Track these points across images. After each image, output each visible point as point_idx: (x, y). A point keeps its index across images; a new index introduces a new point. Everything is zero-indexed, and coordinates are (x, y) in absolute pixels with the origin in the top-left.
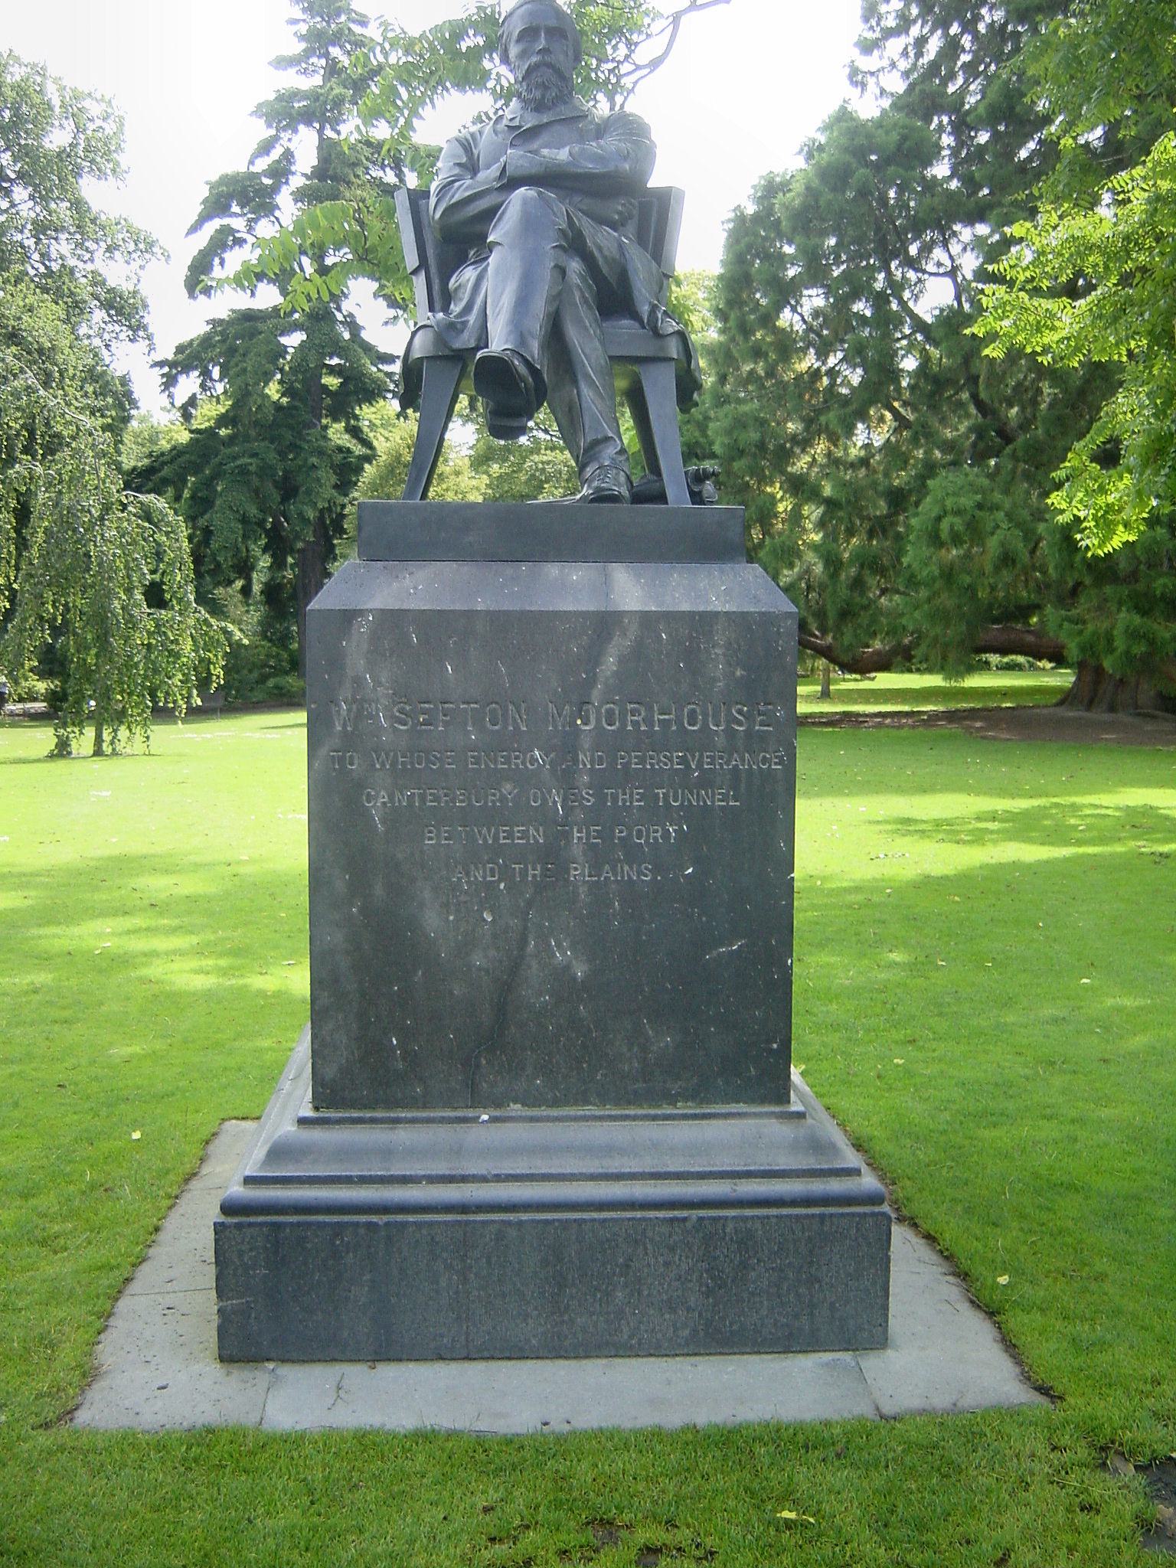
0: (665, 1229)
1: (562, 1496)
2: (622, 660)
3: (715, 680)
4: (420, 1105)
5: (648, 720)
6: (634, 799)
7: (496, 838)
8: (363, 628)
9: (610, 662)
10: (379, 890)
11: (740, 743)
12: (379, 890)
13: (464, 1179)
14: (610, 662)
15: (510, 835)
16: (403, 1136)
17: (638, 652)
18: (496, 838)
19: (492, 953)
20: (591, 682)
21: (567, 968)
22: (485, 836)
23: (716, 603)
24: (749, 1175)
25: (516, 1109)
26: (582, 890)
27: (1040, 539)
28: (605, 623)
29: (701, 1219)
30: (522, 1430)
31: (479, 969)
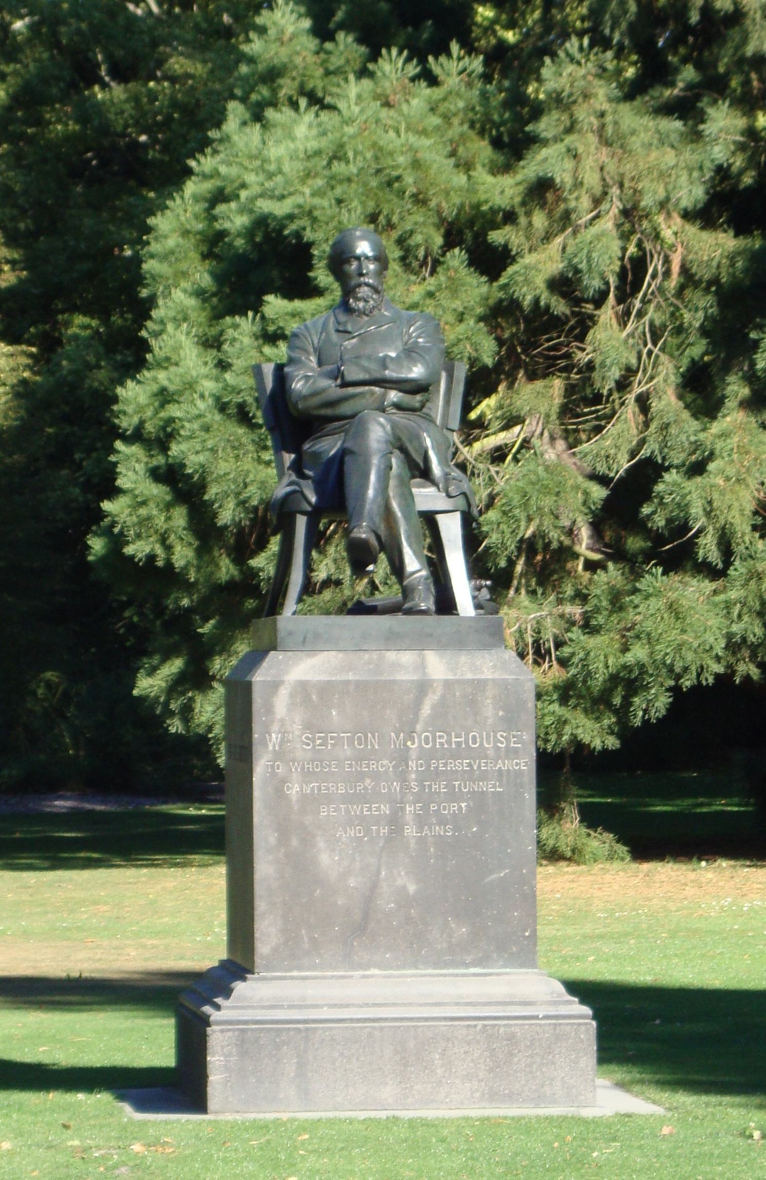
2: (434, 707)
3: (487, 718)
5: (449, 742)
7: (362, 812)
11: (503, 754)
14: (426, 710)
20: (416, 720)
21: (404, 887)
22: (356, 810)
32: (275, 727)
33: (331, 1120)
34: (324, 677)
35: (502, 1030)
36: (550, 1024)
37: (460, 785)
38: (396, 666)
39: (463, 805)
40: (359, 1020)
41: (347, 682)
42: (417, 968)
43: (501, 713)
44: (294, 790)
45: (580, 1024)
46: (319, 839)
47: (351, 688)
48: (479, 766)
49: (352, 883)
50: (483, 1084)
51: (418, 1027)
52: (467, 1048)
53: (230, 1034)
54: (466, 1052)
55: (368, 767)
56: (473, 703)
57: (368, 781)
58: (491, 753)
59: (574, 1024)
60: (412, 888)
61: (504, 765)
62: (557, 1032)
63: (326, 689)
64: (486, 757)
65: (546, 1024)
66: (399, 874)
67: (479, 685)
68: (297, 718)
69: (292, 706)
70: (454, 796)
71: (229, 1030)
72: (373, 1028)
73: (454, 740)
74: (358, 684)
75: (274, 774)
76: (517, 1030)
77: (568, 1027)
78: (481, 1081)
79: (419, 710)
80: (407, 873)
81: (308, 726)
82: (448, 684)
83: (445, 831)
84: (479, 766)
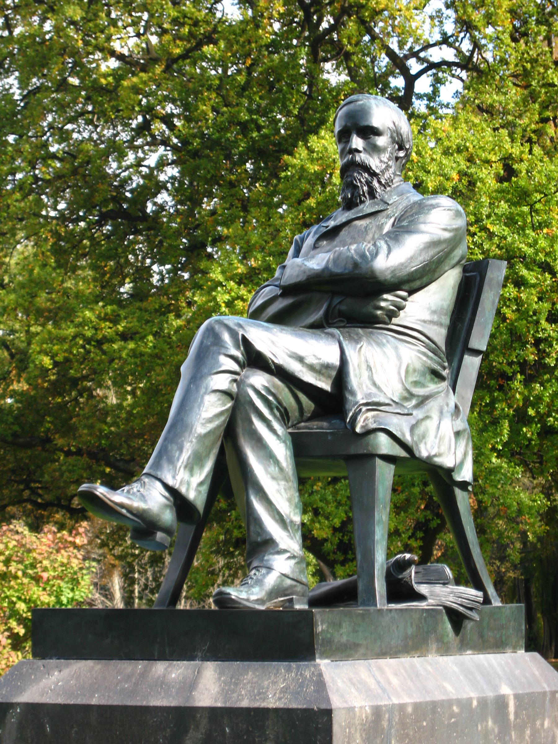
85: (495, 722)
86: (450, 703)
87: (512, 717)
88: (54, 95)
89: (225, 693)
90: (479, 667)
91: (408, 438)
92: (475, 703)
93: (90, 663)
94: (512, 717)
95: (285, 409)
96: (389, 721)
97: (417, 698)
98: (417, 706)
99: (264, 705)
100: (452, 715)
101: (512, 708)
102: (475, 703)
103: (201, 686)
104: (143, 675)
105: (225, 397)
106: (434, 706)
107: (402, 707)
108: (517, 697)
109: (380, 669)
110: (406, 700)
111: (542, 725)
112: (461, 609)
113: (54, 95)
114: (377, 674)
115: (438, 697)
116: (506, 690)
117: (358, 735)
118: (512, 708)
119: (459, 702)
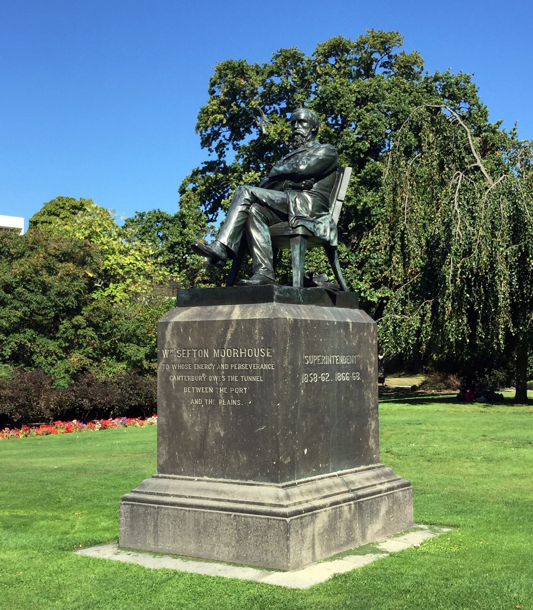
0: (226, 518)
1: (89, 581)
2: (232, 335)
3: (256, 340)
4: (331, 470)
5: (239, 354)
6: (234, 378)
7: (201, 391)
8: (170, 327)
9: (229, 336)
10: (173, 406)
11: (263, 361)
12: (173, 406)
13: (181, 496)
14: (229, 336)
15: (204, 390)
16: (172, 483)
17: (235, 333)
18: (201, 391)
19: (200, 427)
20: (224, 342)
21: (219, 433)
22: (198, 390)
23: (258, 316)
24: (254, 503)
25: (206, 478)
26: (223, 408)
27: (54, 351)
28: (227, 323)
29: (235, 515)
30: (301, 587)
31: (197, 432)
32: (166, 346)
33: (124, 564)
34: (186, 320)
35: (243, 518)
36: (266, 518)
37: (244, 378)
38: (220, 313)
39: (245, 389)
40: (338, 494)
41: (196, 322)
42: (224, 478)
43: (262, 338)
44: (174, 379)
45: (280, 520)
46: (183, 404)
47: (197, 325)
48: (252, 367)
49: (197, 429)
50: (234, 549)
51: (205, 512)
52: (227, 528)
53: (127, 506)
54: (227, 529)
55: (204, 367)
56: (250, 334)
57: (204, 375)
58: (257, 360)
59: (277, 520)
60: (222, 433)
61: (266, 367)
62: (269, 523)
63: (187, 325)
64: (255, 362)
65: (264, 518)
66: (217, 426)
67: (252, 322)
68: (175, 341)
69: (173, 335)
70: (241, 384)
71: (127, 504)
72: (186, 510)
73: (241, 353)
74: (200, 323)
75: (165, 370)
76: (250, 520)
77: (275, 521)
78: (233, 547)
79: (226, 336)
80: (220, 426)
81: (179, 346)
82: (238, 322)
83: (237, 403)
84: (252, 367)
85: (344, 330)
86: (326, 321)
87: (351, 330)
88: (460, 270)
89: (242, 315)
90: (339, 313)
91: (312, 230)
92: (336, 323)
93: (197, 307)
94: (351, 330)
95: (267, 218)
96: (301, 324)
97: (312, 318)
98: (311, 321)
99: (255, 318)
100: (327, 326)
101: (351, 327)
102: (336, 323)
103: (234, 313)
104: (215, 310)
105: (245, 214)
106: (319, 322)
107: (306, 321)
108: (353, 323)
109: (299, 308)
110: (308, 318)
111: (364, 334)
112: (331, 291)
113: (460, 270)
114: (297, 309)
115: (320, 319)
116: (348, 320)
117: (288, 328)
118: (351, 327)
119: (329, 322)
